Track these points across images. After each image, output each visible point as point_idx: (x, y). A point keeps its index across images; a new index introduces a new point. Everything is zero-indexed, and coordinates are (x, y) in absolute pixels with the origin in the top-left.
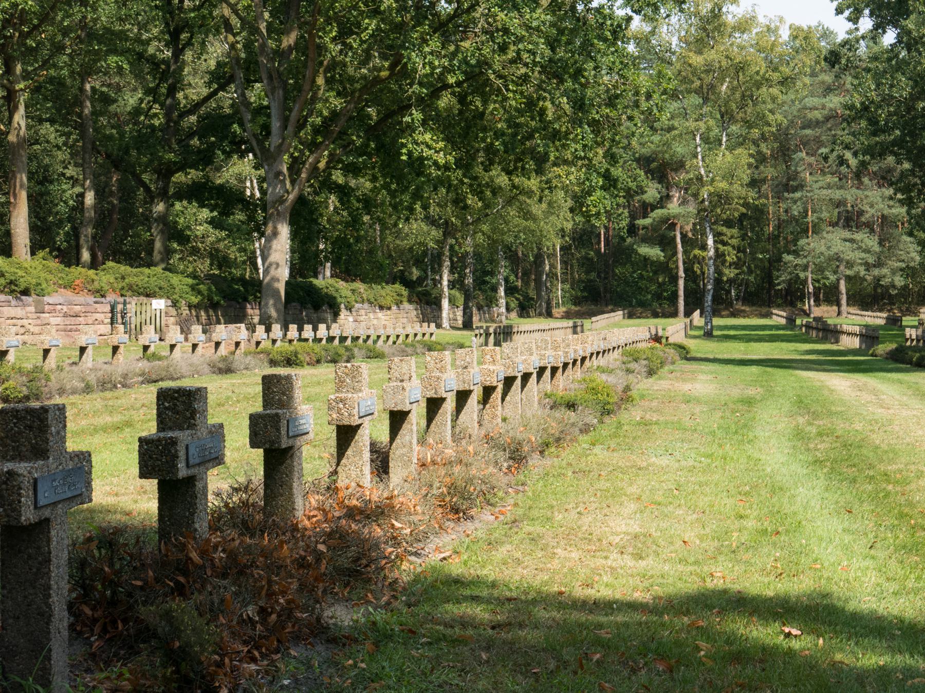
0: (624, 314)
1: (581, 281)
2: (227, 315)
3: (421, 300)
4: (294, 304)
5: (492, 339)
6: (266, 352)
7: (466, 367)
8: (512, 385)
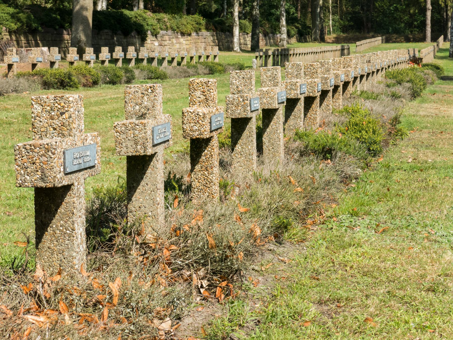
0: (382, 40)
1: (348, 13)
2: (45, 40)
3: (216, 28)
4: (106, 31)
5: (270, 60)
6: (41, 75)
7: (143, 116)
8: (244, 129)
